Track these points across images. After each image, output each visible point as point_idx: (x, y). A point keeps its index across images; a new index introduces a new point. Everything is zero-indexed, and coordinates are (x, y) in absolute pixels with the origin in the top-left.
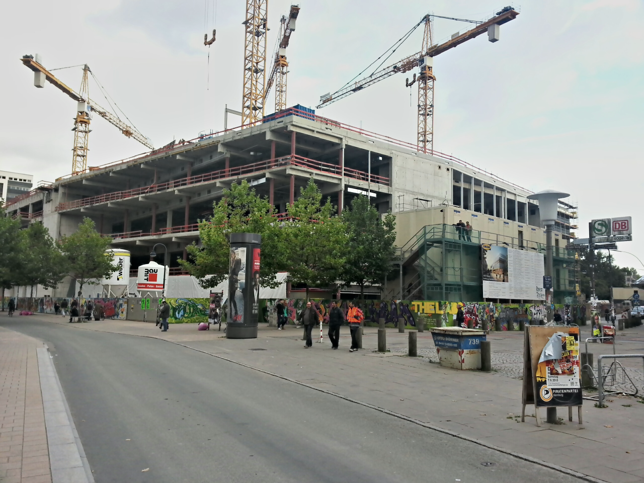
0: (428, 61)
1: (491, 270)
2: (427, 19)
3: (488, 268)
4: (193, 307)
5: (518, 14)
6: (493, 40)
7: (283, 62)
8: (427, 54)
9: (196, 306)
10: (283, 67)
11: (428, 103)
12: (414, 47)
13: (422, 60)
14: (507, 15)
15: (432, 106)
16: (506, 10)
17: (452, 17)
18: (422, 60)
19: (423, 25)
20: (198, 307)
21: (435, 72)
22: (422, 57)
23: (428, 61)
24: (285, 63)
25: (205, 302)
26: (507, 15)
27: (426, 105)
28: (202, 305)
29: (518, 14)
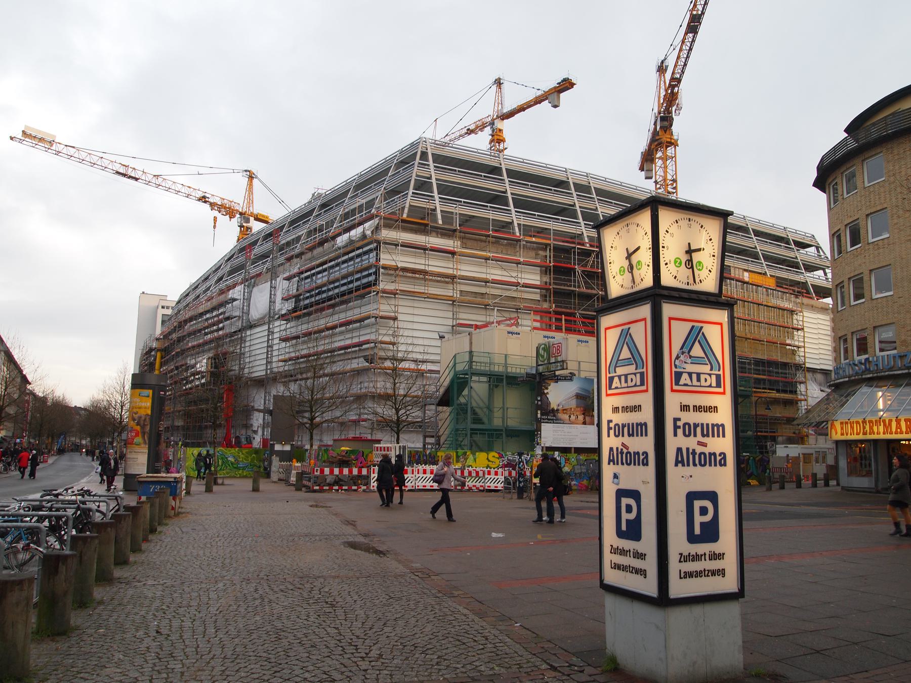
0: (499, 124)
1: (558, 410)
2: (498, 83)
3: (552, 407)
4: (222, 459)
5: (575, 84)
6: (555, 106)
7: (498, 138)
8: (498, 117)
9: (226, 458)
10: (499, 143)
11: (669, 177)
12: (486, 110)
13: (492, 123)
14: (566, 85)
15: (675, 181)
16: (565, 80)
17: (678, 127)
18: (492, 123)
19: (494, 87)
20: (229, 459)
21: (506, 134)
22: (493, 120)
23: (499, 124)
24: (501, 138)
25: (237, 454)
26: (566, 85)
27: (665, 180)
28: (234, 457)
29: (575, 84)
